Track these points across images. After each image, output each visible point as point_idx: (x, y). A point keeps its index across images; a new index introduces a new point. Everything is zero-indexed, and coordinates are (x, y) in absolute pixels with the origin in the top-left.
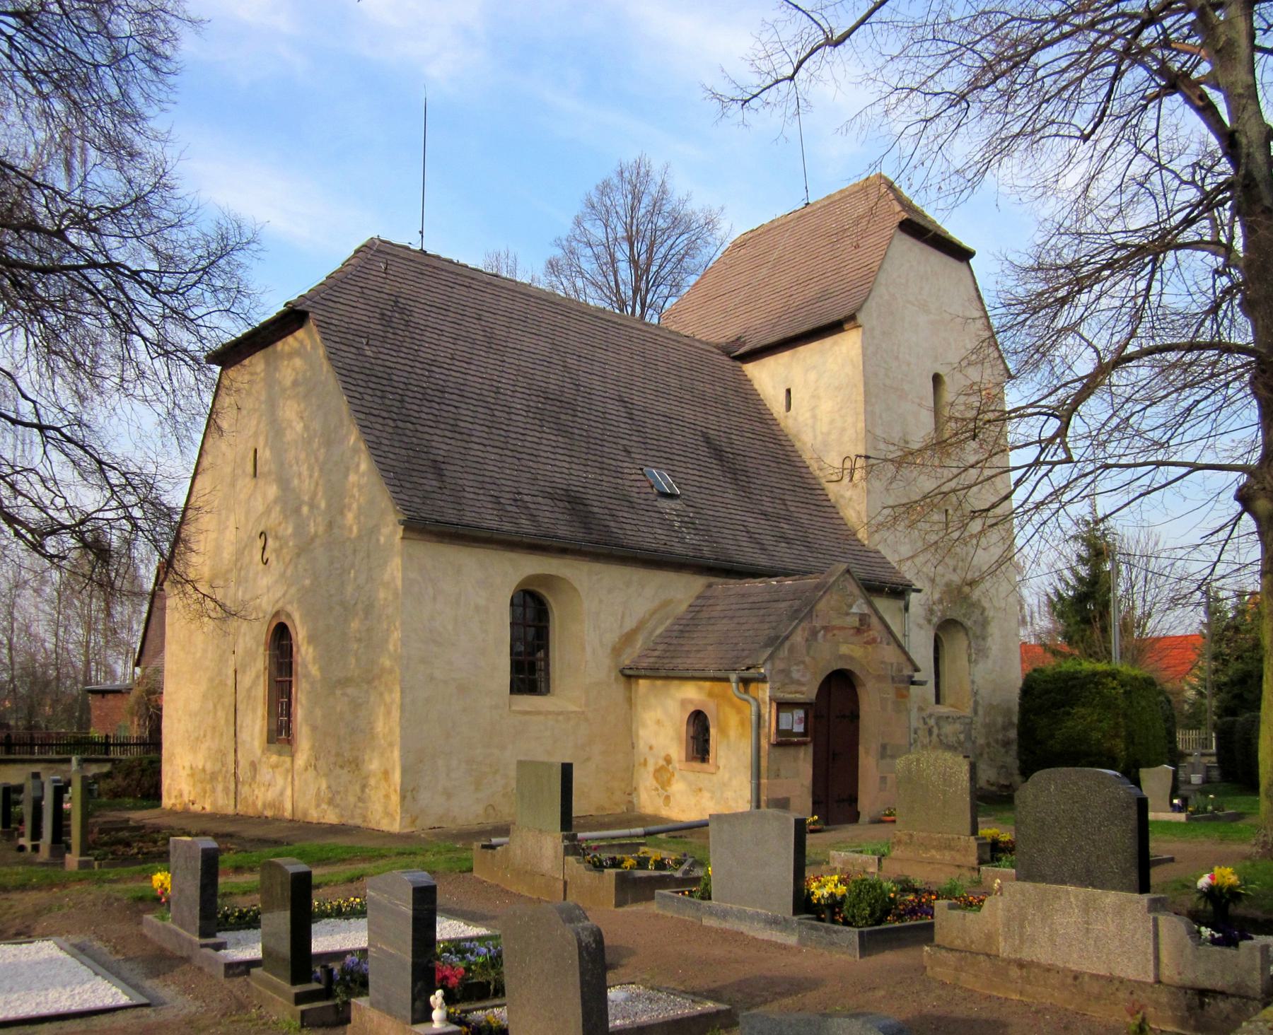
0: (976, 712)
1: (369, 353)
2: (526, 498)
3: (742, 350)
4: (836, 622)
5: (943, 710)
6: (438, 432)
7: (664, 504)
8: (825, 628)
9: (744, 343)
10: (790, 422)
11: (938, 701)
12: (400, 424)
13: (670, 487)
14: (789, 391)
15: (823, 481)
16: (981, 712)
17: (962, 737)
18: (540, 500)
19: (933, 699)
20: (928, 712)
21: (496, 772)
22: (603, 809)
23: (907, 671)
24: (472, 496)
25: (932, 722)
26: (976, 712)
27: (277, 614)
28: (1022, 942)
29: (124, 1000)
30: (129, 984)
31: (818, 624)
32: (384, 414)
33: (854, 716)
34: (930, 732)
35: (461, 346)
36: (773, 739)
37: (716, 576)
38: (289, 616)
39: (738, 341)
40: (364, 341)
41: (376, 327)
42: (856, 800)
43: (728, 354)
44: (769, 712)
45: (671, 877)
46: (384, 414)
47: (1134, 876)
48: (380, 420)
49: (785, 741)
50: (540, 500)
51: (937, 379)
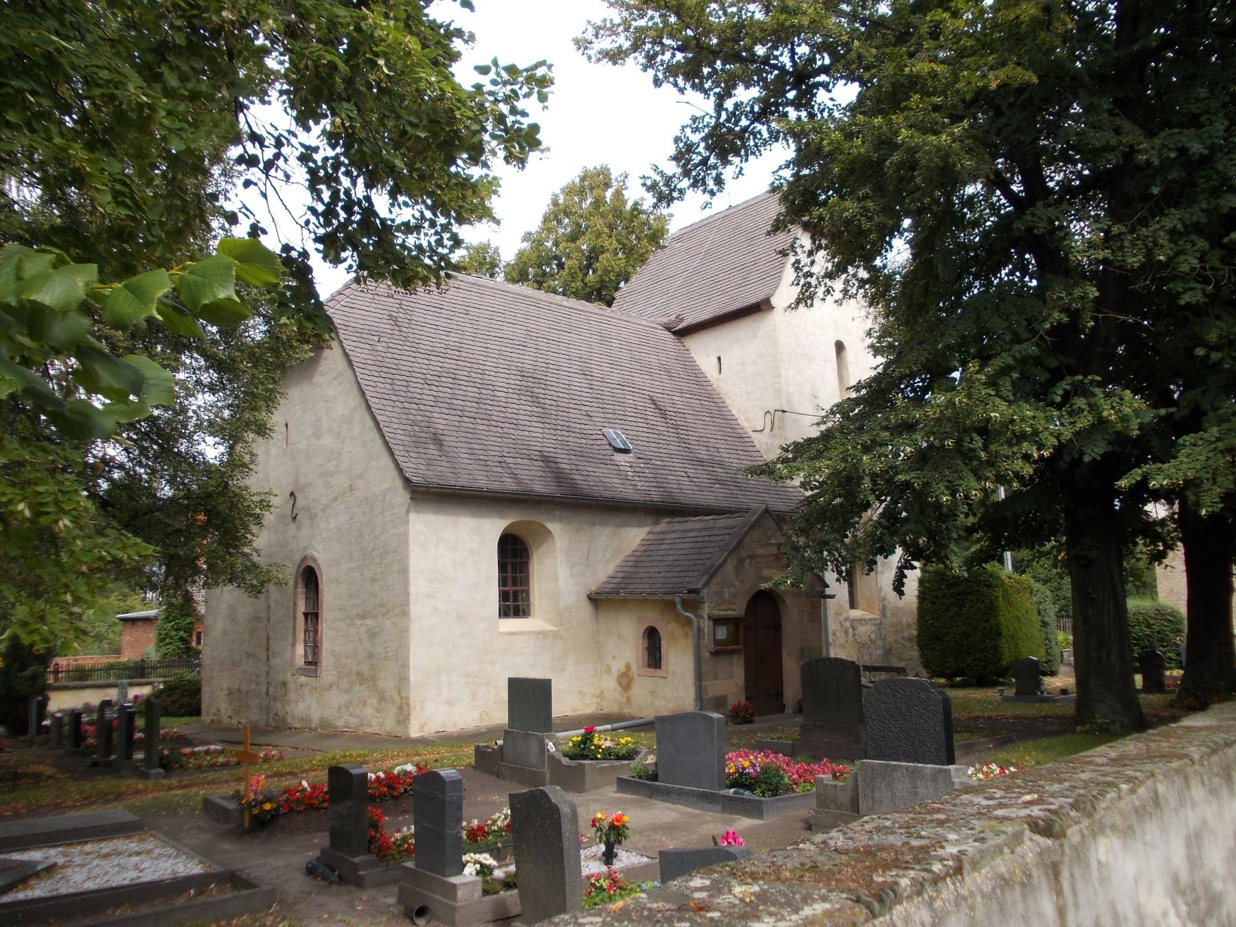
0: (884, 614)
1: (380, 348)
2: (508, 460)
3: (680, 326)
4: (760, 551)
5: (856, 613)
6: (437, 410)
7: (619, 457)
8: (751, 557)
9: (682, 320)
10: (722, 384)
11: (853, 605)
12: (406, 405)
13: (625, 443)
14: (719, 359)
15: (749, 431)
16: (888, 615)
17: (873, 636)
18: (519, 461)
19: (848, 606)
20: (844, 615)
21: (488, 684)
22: (575, 710)
23: (818, 589)
24: (466, 461)
25: (848, 624)
26: (884, 614)
27: (305, 559)
28: (874, 803)
29: (194, 868)
30: (203, 853)
31: (744, 554)
32: (394, 398)
33: (777, 627)
34: (846, 632)
35: (454, 338)
36: (712, 647)
37: (634, 793)
38: (315, 560)
39: (680, 319)
40: (376, 338)
41: (386, 327)
42: (782, 695)
43: (669, 329)
44: (706, 625)
45: (386, 65)
46: (394, 398)
47: (943, 755)
48: (392, 403)
49: (720, 651)
50: (519, 461)
51: (840, 347)
